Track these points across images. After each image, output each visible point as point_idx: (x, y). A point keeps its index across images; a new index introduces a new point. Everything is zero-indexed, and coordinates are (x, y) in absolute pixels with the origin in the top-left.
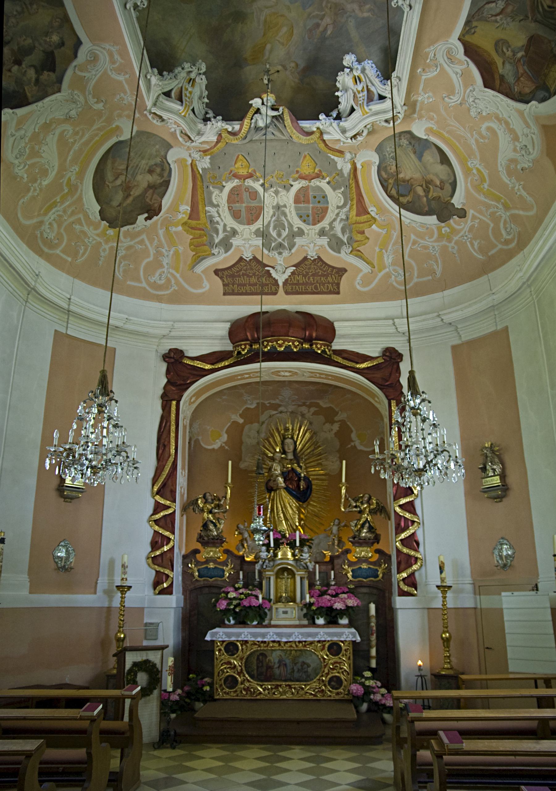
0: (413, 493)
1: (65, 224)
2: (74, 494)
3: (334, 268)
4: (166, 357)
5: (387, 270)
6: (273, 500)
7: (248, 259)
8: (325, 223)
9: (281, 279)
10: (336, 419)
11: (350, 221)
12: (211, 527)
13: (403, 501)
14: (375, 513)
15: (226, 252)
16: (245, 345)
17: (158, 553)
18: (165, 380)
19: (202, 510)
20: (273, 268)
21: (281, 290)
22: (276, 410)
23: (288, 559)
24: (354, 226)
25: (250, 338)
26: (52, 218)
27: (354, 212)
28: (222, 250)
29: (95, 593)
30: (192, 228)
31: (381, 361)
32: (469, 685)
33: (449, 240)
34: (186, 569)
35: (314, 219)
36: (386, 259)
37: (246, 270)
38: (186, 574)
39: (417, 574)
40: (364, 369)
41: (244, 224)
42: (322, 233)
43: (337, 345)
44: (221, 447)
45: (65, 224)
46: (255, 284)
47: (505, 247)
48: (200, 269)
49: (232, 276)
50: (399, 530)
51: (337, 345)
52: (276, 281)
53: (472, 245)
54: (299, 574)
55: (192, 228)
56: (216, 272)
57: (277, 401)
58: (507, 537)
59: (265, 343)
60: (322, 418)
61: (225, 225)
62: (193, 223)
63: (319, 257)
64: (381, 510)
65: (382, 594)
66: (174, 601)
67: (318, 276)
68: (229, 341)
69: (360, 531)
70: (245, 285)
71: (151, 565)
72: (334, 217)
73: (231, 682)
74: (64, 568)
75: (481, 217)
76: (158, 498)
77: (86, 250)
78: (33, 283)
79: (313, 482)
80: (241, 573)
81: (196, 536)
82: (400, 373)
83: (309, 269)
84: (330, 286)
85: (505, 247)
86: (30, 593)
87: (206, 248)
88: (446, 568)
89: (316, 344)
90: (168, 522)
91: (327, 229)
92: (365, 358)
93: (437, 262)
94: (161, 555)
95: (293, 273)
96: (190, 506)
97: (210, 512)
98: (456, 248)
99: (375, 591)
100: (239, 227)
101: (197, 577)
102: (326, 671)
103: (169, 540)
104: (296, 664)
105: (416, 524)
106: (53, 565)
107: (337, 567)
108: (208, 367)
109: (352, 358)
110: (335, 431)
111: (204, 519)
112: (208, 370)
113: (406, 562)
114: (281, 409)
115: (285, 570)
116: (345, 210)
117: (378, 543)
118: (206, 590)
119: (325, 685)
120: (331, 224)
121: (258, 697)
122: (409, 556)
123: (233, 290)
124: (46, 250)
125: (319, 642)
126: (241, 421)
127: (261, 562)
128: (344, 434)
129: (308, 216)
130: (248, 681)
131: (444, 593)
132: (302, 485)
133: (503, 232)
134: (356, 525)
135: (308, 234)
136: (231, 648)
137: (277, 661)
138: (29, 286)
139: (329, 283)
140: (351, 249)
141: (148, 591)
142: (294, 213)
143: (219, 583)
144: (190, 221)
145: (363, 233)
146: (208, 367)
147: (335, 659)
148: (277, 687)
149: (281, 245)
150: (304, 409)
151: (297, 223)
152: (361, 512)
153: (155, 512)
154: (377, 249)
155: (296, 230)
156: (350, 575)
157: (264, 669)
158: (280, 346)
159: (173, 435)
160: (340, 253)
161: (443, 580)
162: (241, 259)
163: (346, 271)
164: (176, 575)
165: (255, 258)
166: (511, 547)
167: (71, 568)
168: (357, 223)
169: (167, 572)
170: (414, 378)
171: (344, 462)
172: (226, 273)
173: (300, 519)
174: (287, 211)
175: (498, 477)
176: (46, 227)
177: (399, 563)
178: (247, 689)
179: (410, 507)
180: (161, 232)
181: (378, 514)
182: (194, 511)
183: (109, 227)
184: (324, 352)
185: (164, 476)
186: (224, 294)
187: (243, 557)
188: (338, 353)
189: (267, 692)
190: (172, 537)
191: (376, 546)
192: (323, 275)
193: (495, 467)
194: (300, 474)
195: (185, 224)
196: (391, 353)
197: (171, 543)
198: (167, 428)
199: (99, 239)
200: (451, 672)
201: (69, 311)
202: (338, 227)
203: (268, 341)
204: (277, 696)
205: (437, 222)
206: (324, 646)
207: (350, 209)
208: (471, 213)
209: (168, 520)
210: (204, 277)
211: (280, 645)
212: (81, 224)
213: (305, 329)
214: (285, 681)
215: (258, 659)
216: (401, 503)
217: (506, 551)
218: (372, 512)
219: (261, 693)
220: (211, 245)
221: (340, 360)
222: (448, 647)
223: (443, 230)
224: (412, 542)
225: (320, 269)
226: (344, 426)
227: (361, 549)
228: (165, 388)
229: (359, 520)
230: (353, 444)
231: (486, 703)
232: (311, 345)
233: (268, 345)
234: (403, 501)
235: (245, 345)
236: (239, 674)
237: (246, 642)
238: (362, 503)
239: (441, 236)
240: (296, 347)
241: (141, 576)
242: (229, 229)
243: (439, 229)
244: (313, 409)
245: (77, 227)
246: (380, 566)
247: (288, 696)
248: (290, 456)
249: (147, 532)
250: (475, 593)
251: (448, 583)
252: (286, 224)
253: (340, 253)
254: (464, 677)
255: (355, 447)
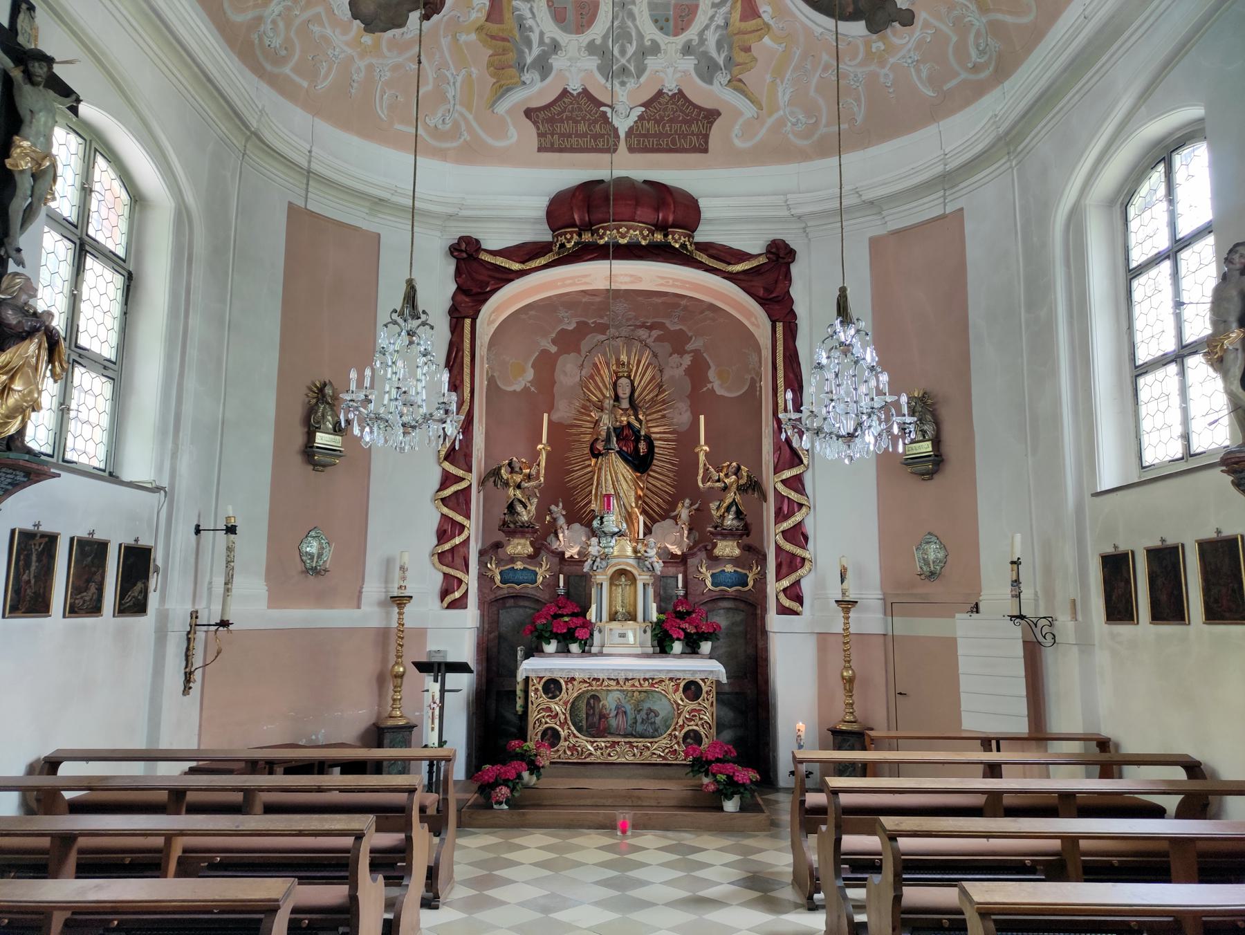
0: (802, 462)
1: (298, 22)
2: (328, 460)
3: (701, 109)
4: (454, 250)
5: (781, 113)
6: (600, 469)
7: (575, 93)
8: (692, 34)
9: (623, 124)
10: (689, 347)
11: (730, 29)
12: (519, 508)
13: (787, 474)
14: (746, 491)
15: (543, 80)
16: (571, 233)
17: (447, 546)
18: (454, 287)
19: (507, 484)
20: (611, 107)
21: (622, 145)
22: (604, 334)
23: (628, 557)
24: (736, 38)
25: (578, 222)
26: (276, 12)
27: (737, 15)
28: (537, 76)
29: (359, 607)
30: (493, 37)
31: (763, 260)
32: (876, 744)
33: (882, 63)
34: (483, 570)
35: (676, 26)
36: (780, 94)
37: (572, 111)
38: (483, 577)
39: (804, 583)
40: (738, 273)
41: (571, 33)
42: (687, 50)
43: (700, 237)
44: (526, 389)
45: (298, 22)
46: (584, 135)
47: (973, 77)
48: (503, 107)
49: (551, 121)
50: (780, 516)
51: (700, 237)
52: (616, 130)
53: (918, 71)
54: (642, 578)
55: (493, 37)
56: (529, 113)
57: (604, 321)
58: (935, 533)
59: (601, 231)
60: (667, 347)
61: (542, 34)
62: (494, 28)
63: (680, 91)
64: (753, 486)
65: (751, 609)
66: (470, 617)
67: (680, 123)
68: (547, 227)
69: (722, 517)
70: (570, 136)
71: (437, 564)
72: (707, 22)
73: (552, 737)
74: (315, 571)
75: (937, 24)
76: (447, 465)
77: (330, 70)
78: (255, 125)
79: (656, 443)
80: (561, 576)
81: (498, 523)
82: (790, 280)
83: (665, 110)
84: (694, 139)
85: (973, 77)
86: (269, 608)
87: (513, 71)
88: (849, 575)
89: (673, 234)
90: (460, 501)
91: (694, 43)
92: (741, 256)
93: (858, 100)
94: (452, 550)
95: (641, 118)
96: (492, 475)
97: (519, 486)
98: (891, 76)
99: (742, 606)
100: (563, 38)
101: (498, 583)
102: (681, 722)
103: (462, 527)
104: (639, 711)
105: (804, 510)
106: (300, 567)
107: (691, 570)
108: (516, 266)
109: (719, 257)
110: (685, 366)
111: (509, 497)
112: (516, 272)
113: (789, 564)
114: (612, 331)
115: (622, 572)
116: (724, 9)
117: (748, 535)
118: (510, 602)
119: (678, 743)
120: (701, 34)
121: (588, 760)
122: (793, 556)
123: (552, 144)
124: (268, 67)
125: (671, 679)
126: (553, 349)
127: (590, 562)
128: (697, 372)
129: (667, 20)
130: (575, 736)
131: (847, 610)
132: (642, 446)
133: (973, 53)
134: (718, 508)
135: (666, 53)
136: (552, 687)
137: (613, 707)
138: (247, 127)
139: (693, 134)
140: (729, 77)
141: (434, 604)
142: (646, 13)
143: (529, 591)
144: (488, 24)
145: (747, 50)
146: (516, 266)
147: (693, 705)
148: (614, 744)
149: (624, 70)
150: (643, 333)
151: (651, 32)
152: (726, 488)
153: (443, 485)
154: (768, 78)
155: (648, 43)
156: (709, 583)
157: (596, 719)
158: (623, 236)
159: (467, 370)
160: (710, 82)
161: (844, 594)
162: (565, 92)
163: (719, 114)
164: (472, 580)
165: (585, 92)
166: (943, 547)
167: (326, 571)
168: (741, 32)
169: (459, 574)
170: (845, 297)
171: (702, 417)
172: (542, 115)
173: (638, 498)
174: (635, 10)
175: (929, 443)
176: (267, 26)
177: (779, 566)
178: (573, 748)
179: (796, 483)
180: (445, 42)
181: (750, 491)
182: (496, 485)
183: (365, 30)
184: (683, 246)
185: (170, 148)
186: (540, 150)
187: (563, 553)
188: (705, 247)
189: (599, 752)
190: (466, 523)
191: (746, 540)
192: (685, 122)
193: (925, 428)
194: (639, 431)
195: (480, 29)
196: (778, 249)
197: (466, 532)
198: (458, 360)
199: (349, 51)
200: (854, 727)
201: (309, 172)
202: (712, 38)
203: (605, 229)
204: (613, 759)
205: (866, 32)
206: (678, 685)
207: (732, 7)
208: (922, 16)
209: (461, 499)
210: (509, 120)
211: (618, 683)
212: (322, 24)
213: (657, 210)
214: (625, 736)
215: (588, 703)
216: (784, 477)
217: (933, 552)
218: (741, 489)
219: (591, 754)
220: (521, 68)
221: (704, 258)
222: (851, 691)
223: (874, 46)
224: (797, 535)
225: (682, 111)
226: (698, 357)
227: (725, 543)
228: (453, 298)
229: (722, 501)
230: (709, 386)
231: (896, 769)
232: (666, 236)
233: (604, 234)
234: (787, 474)
235: (571, 233)
236: (562, 725)
237: (573, 679)
238: (727, 475)
239: (869, 56)
240: (644, 238)
241: (425, 580)
242: (547, 41)
243: (868, 45)
244: (655, 333)
245: (316, 29)
246: (751, 569)
247: (630, 759)
248: (625, 404)
249: (431, 516)
250: (885, 614)
251: (851, 596)
252: (634, 34)
253: (710, 82)
254: (872, 733)
255: (713, 391)
